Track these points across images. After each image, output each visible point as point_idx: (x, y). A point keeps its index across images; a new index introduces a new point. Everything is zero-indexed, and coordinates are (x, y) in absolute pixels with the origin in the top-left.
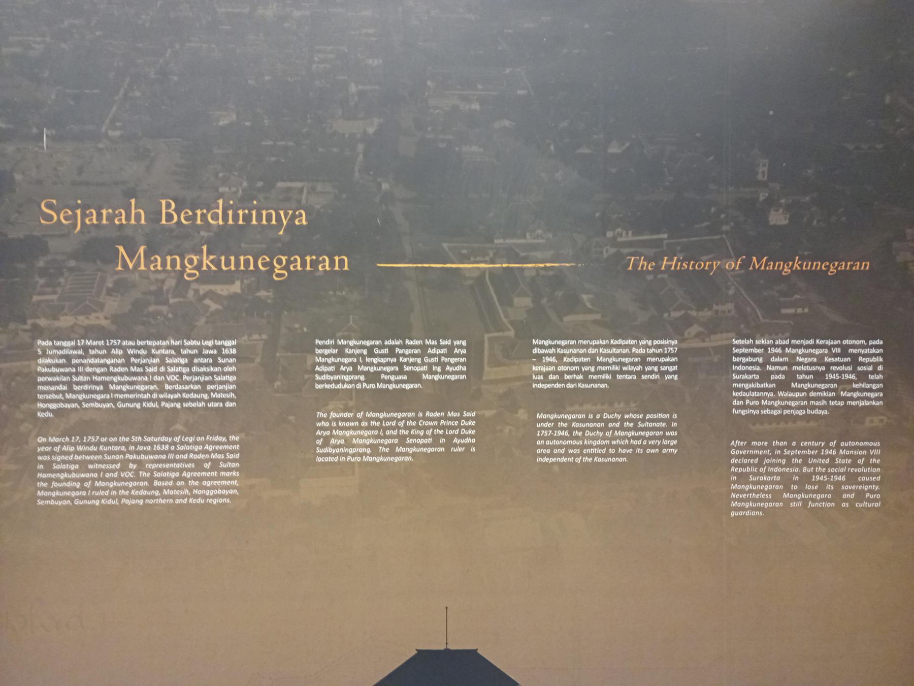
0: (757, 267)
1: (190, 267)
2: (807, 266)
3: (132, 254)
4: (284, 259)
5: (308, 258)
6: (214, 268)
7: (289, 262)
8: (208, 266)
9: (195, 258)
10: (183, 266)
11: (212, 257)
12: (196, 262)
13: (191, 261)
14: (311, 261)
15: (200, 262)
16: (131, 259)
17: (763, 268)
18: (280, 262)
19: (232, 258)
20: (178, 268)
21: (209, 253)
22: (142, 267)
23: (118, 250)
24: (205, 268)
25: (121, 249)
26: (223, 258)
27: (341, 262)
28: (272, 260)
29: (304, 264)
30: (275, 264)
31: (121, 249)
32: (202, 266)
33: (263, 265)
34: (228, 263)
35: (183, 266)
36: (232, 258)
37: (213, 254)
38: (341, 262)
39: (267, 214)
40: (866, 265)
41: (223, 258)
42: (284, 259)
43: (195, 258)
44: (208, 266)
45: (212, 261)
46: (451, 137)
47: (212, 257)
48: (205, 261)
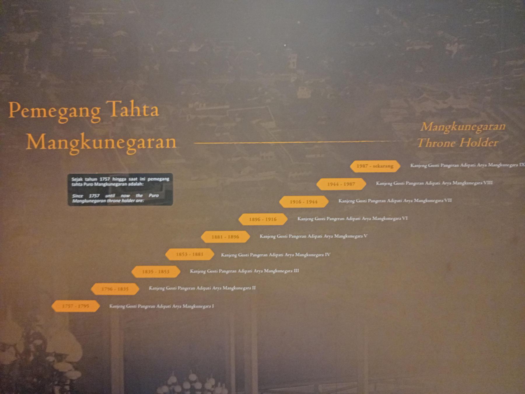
0: (426, 129)
1: (130, 146)
2: (461, 128)
3: (36, 139)
4: (65, 109)
5: (149, 140)
6: (89, 147)
7: (69, 112)
8: (85, 146)
9: (77, 141)
10: (445, 129)
11: (87, 140)
12: (77, 144)
13: (74, 143)
14: (152, 142)
15: (80, 143)
16: (36, 142)
17: (430, 130)
18: (63, 112)
19: (100, 141)
20: (66, 147)
21: (85, 138)
22: (43, 147)
23: (27, 136)
24: (83, 148)
25: (30, 136)
26: (94, 141)
27: (171, 143)
28: (126, 141)
29: (146, 144)
30: (128, 145)
31: (30, 136)
32: (81, 146)
33: (120, 145)
34: (97, 145)
35: (445, 129)
36: (100, 141)
37: (88, 139)
38: (171, 143)
39: (170, 141)
40: (503, 127)
41: (94, 141)
42: (65, 109)
43: (77, 141)
44: (85, 146)
45: (87, 143)
46: (85, 43)
47: (87, 140)
48: (83, 143)
